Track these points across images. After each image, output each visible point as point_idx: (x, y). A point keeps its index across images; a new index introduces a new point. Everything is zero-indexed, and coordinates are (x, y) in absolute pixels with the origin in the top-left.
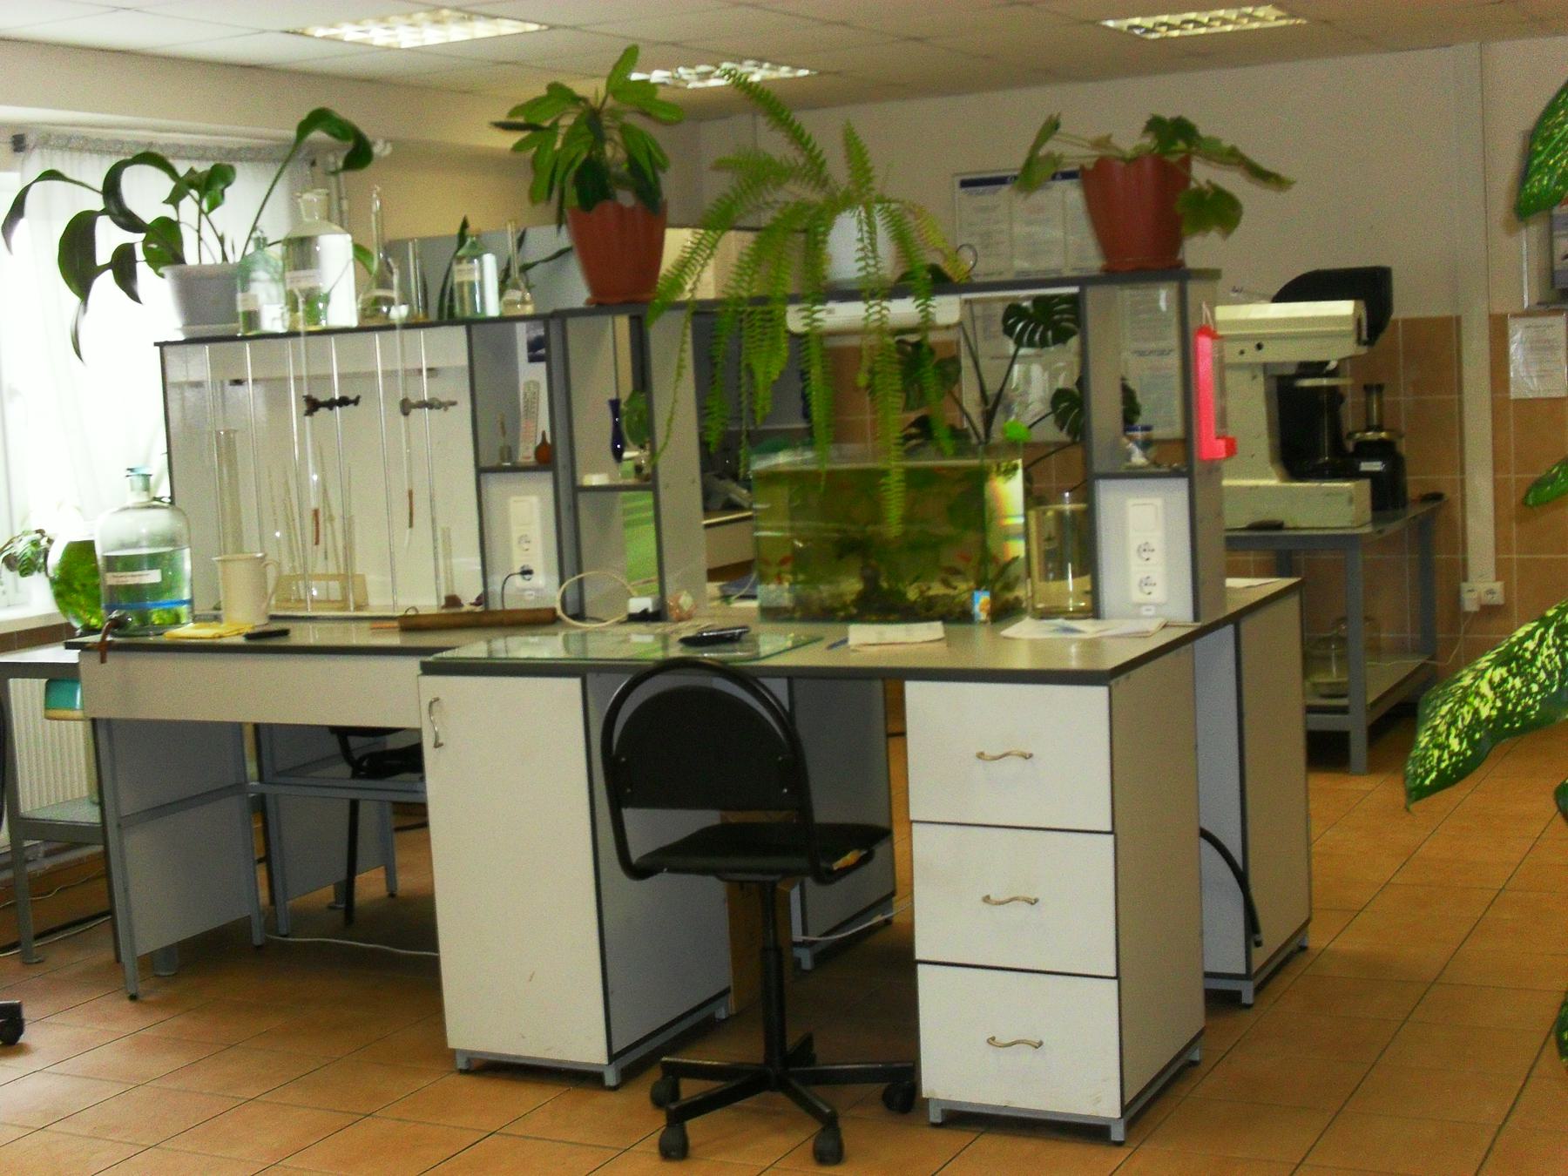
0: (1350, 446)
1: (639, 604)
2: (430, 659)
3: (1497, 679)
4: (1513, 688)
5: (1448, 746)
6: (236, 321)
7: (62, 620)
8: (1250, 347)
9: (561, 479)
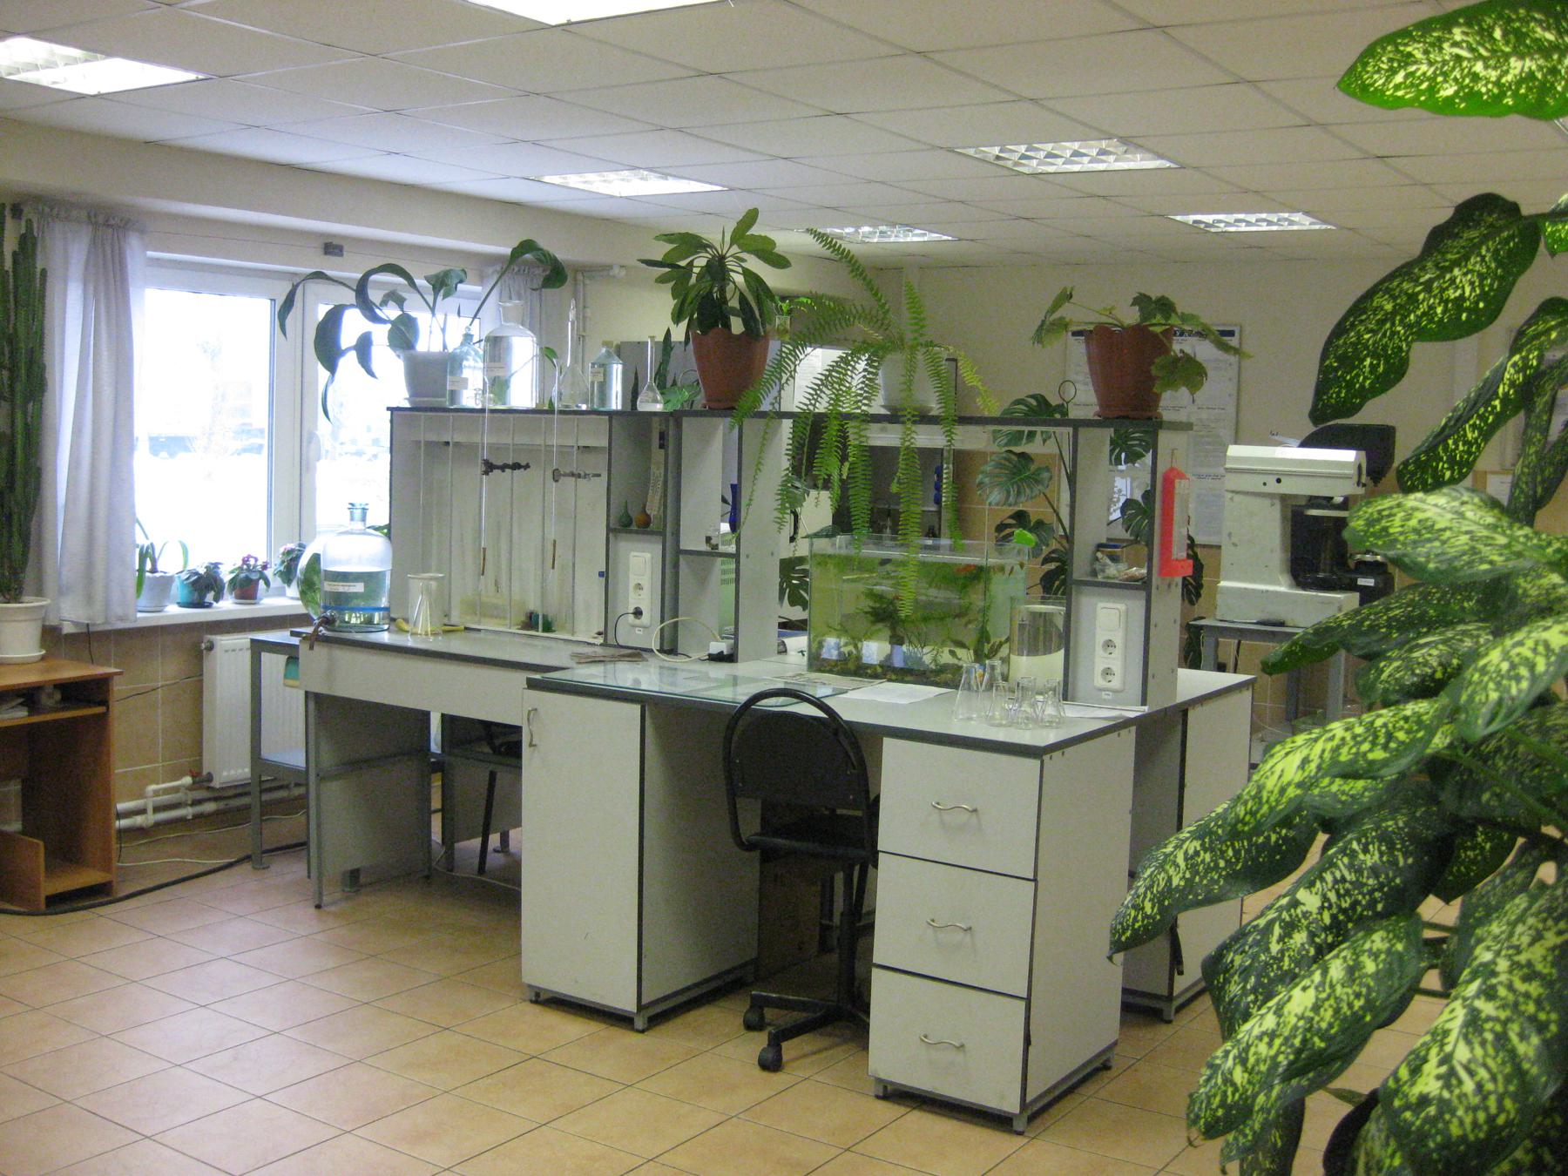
0: (1351, 564)
1: (720, 646)
2: (538, 676)
3: (1191, 852)
4: (1203, 861)
5: (1143, 908)
6: (444, 396)
7: (303, 610)
8: (1272, 480)
9: (668, 544)
